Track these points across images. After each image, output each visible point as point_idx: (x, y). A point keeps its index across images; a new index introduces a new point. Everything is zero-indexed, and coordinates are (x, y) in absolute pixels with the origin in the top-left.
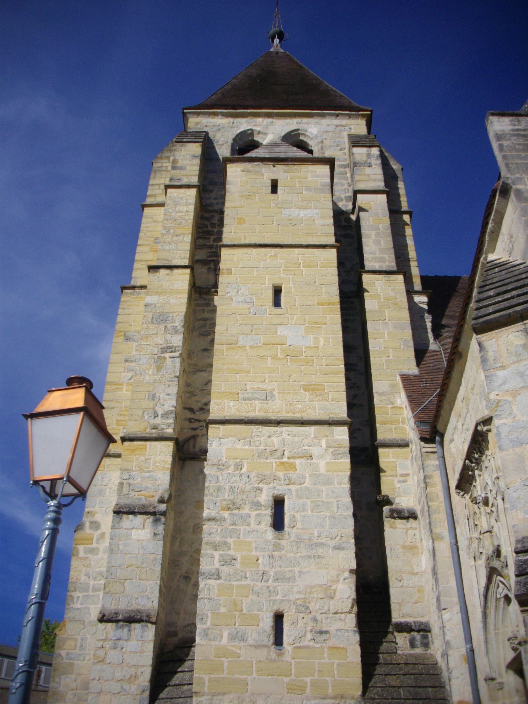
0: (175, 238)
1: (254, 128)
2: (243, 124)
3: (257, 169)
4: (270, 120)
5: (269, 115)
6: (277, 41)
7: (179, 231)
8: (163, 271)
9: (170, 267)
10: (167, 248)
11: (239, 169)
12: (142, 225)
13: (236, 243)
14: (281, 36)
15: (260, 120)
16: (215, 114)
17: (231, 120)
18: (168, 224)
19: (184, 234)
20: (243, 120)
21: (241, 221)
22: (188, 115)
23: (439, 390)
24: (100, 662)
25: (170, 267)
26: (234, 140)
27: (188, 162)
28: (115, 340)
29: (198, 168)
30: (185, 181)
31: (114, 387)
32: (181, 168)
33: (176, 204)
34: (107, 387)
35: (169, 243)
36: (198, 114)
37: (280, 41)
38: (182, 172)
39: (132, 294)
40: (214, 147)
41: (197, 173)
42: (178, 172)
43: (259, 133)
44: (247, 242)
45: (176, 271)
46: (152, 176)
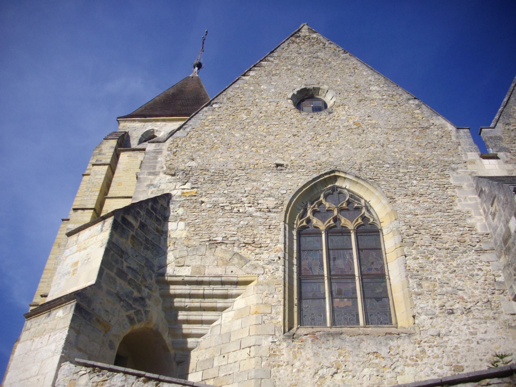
0: (91, 193)
1: (155, 128)
2: (149, 126)
3: (136, 155)
4: (164, 123)
5: (164, 121)
6: (197, 68)
7: (94, 189)
8: (80, 211)
9: (83, 209)
10: (86, 199)
11: (126, 156)
12: (81, 186)
13: (113, 196)
14: (199, 66)
15: (159, 123)
16: (135, 121)
17: (143, 124)
18: (89, 185)
19: (96, 191)
20: (149, 124)
21: (120, 184)
22: (120, 122)
23: (302, 210)
24: (22, 380)
25: (83, 209)
26: (142, 135)
27: (108, 151)
28: (53, 247)
29: (112, 154)
30: (104, 162)
31: (48, 271)
32: (103, 154)
33: (96, 174)
34: (45, 271)
35: (88, 196)
36: (125, 121)
37: (198, 69)
38: (104, 156)
39: (67, 223)
40: (129, 140)
41: (111, 157)
42: (101, 156)
43: (157, 131)
44: (120, 195)
45: (86, 211)
46: (92, 158)
